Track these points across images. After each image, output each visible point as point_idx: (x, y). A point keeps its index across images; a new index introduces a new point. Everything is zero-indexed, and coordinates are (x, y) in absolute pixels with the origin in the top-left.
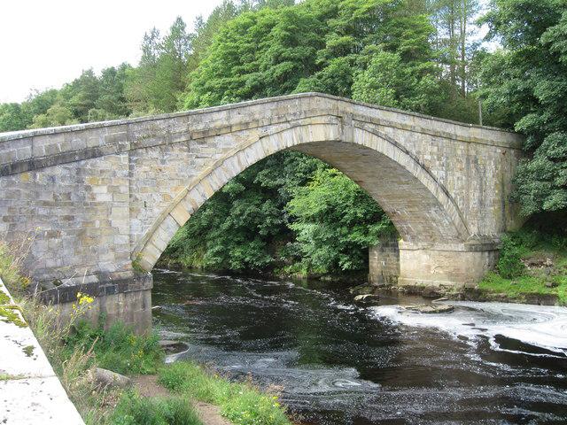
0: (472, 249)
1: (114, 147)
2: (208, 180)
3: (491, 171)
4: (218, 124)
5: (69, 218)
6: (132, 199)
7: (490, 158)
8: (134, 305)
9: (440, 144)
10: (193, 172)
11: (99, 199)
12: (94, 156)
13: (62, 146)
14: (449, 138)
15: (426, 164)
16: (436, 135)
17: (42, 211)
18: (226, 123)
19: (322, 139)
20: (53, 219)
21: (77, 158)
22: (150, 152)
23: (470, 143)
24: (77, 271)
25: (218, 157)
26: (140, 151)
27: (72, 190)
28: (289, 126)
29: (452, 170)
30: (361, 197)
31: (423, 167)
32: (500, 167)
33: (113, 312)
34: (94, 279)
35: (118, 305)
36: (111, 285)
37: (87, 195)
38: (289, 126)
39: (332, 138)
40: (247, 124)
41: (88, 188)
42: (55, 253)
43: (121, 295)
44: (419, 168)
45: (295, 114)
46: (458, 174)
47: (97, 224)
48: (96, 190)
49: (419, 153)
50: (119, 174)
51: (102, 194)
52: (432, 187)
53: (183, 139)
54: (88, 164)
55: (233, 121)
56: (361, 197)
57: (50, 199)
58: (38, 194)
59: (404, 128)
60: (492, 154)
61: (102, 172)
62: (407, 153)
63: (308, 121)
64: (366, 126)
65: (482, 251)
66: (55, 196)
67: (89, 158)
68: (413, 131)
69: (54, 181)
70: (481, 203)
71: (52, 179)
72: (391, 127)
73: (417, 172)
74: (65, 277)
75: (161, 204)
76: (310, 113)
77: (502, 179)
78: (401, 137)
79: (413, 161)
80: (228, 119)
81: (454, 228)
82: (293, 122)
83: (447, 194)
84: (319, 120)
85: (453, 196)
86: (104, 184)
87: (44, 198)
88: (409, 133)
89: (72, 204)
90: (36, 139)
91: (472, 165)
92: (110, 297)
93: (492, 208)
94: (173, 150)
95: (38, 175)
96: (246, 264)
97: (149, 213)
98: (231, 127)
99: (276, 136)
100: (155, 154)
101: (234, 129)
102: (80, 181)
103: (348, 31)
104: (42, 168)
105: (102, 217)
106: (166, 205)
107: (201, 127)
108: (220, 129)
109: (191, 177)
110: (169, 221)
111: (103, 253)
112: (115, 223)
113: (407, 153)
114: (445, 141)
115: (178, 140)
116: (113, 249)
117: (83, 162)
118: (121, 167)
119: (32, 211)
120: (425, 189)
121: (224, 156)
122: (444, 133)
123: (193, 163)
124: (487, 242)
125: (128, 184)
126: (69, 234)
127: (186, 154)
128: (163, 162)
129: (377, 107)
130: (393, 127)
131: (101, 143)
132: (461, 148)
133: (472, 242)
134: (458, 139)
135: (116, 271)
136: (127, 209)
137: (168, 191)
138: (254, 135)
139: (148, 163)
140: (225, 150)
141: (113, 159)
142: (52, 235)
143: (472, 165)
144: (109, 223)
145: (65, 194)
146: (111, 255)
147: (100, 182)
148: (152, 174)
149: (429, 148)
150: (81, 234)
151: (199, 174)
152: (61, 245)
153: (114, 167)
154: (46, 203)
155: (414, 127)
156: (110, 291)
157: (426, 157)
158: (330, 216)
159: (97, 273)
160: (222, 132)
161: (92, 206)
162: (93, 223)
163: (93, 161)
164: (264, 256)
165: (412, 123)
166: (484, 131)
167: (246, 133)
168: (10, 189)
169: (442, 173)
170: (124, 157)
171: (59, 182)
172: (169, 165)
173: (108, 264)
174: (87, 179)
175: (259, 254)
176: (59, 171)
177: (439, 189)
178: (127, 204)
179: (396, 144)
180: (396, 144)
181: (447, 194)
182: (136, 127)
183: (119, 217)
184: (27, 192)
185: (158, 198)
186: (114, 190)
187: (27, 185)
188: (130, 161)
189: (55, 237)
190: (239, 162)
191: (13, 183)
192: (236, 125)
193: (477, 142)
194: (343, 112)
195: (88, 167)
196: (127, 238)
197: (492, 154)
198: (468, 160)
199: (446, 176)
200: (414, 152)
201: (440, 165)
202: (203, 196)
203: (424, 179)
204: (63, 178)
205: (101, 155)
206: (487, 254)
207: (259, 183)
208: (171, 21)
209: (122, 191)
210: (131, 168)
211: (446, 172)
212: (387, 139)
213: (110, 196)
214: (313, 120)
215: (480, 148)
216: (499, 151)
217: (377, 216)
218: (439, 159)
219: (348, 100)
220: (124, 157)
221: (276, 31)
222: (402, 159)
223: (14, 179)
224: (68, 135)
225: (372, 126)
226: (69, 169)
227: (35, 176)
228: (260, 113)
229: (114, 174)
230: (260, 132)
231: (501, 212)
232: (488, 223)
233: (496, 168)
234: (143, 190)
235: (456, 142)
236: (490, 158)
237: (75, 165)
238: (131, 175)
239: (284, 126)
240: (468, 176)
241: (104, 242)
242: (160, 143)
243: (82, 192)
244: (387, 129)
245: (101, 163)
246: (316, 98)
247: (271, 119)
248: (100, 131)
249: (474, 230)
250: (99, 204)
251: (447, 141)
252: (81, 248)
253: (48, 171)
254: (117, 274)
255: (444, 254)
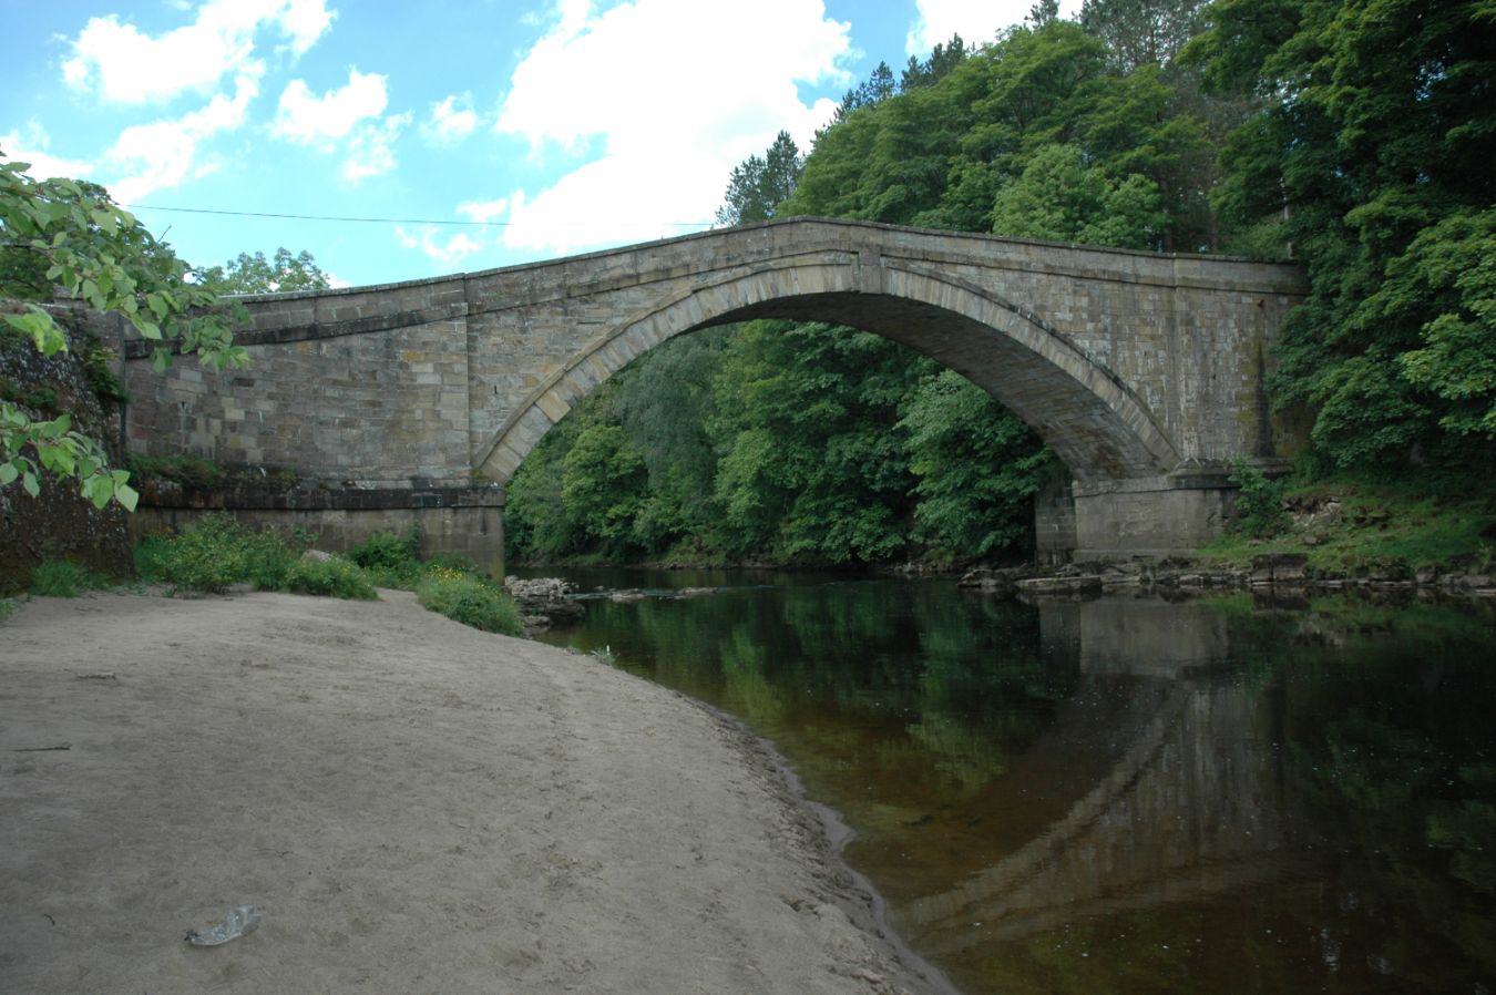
0: (1183, 483)
1: (444, 311)
2: (600, 357)
3: (1229, 341)
4: (617, 273)
5: (373, 404)
6: (475, 383)
7: (1225, 314)
8: (469, 526)
9: (1096, 293)
10: (575, 345)
11: (421, 380)
12: (412, 323)
13: (363, 310)
14: (1121, 280)
15: (1062, 329)
16: (1082, 276)
17: (330, 392)
18: (631, 271)
19: (820, 289)
20: (349, 403)
21: (385, 325)
22: (503, 317)
23: (1174, 288)
24: (382, 473)
25: (617, 321)
26: (487, 315)
27: (378, 367)
28: (749, 271)
29: (1131, 338)
30: (998, 410)
31: (1053, 333)
32: (1251, 330)
33: (438, 533)
34: (407, 485)
35: (443, 523)
36: (431, 494)
37: (402, 374)
38: (749, 271)
39: (839, 286)
40: (668, 270)
41: (403, 366)
42: (352, 449)
43: (448, 511)
44: (1044, 337)
45: (760, 253)
46: (1148, 346)
47: (418, 414)
48: (415, 368)
49: (1042, 308)
50: (452, 348)
51: (426, 374)
52: (1077, 370)
53: (555, 296)
54: (404, 334)
55: (641, 269)
56: (998, 410)
57: (345, 377)
58: (324, 370)
59: (1002, 266)
60: (1232, 306)
61: (425, 344)
62: (1012, 309)
63: (788, 262)
64: (912, 266)
65: (1205, 489)
66: (350, 374)
67: (404, 326)
68: (1024, 269)
69: (349, 354)
70: (1205, 398)
71: (348, 352)
72: (972, 265)
73: (1040, 343)
74: (363, 479)
75: (521, 391)
76: (794, 250)
77: (1260, 353)
78: (997, 283)
79: (1027, 323)
80: (634, 264)
81: (1141, 447)
82: (757, 265)
83: (1116, 381)
84: (809, 260)
85: (1134, 386)
86: (426, 361)
87: (333, 375)
88: (1017, 274)
89: (379, 386)
90: (320, 301)
91: (1180, 329)
92: (430, 512)
93: (1235, 410)
94: (539, 313)
95: (325, 346)
96: (855, 550)
97: (503, 403)
98: (638, 276)
99: (725, 289)
100: (511, 319)
101: (643, 280)
102: (391, 356)
103: (1001, 114)
104: (330, 337)
105: (428, 405)
106: (529, 391)
107: (586, 279)
108: (618, 280)
109: (570, 351)
110: (535, 413)
111: (428, 454)
112: (446, 414)
113: (1012, 309)
114: (1107, 286)
115: (547, 299)
116: (444, 450)
117: (395, 332)
118: (455, 338)
119: (315, 392)
120: (1063, 373)
121: (627, 320)
122: (1104, 272)
123: (573, 331)
124: (1215, 471)
125: (465, 361)
126: (373, 424)
127: (560, 318)
128: (524, 330)
129: (956, 233)
130: (979, 266)
131: (424, 305)
132: (1149, 301)
133: (1179, 472)
134: (1141, 281)
135: (443, 479)
136: (464, 396)
137: (532, 371)
138: (683, 288)
139: (500, 332)
140: (628, 312)
141: (442, 327)
142: (345, 424)
143: (1180, 329)
144: (437, 415)
145: (366, 372)
146: (442, 457)
147: (422, 358)
148: (506, 348)
149: (1068, 301)
150: (394, 425)
151: (585, 348)
152: (361, 438)
153: (444, 338)
154: (336, 383)
155: (1028, 264)
156: (430, 504)
157: (1059, 315)
158: (956, 444)
159: (414, 479)
160: (622, 285)
161: (411, 390)
162: (412, 412)
163: (409, 329)
164: (886, 534)
165: (1023, 257)
166: (1208, 265)
167: (666, 285)
168: (280, 360)
169: (1105, 344)
170: (459, 326)
171: (357, 356)
172: (532, 334)
173: (436, 470)
174: (402, 354)
175: (880, 530)
176: (357, 341)
177: (1096, 374)
178: (465, 388)
179: (983, 294)
180: (983, 294)
181: (1116, 381)
182: (481, 284)
183: (453, 405)
184: (308, 366)
185: (516, 382)
186: (443, 369)
187: (306, 358)
188: (469, 329)
189: (352, 427)
190: (656, 329)
191: (284, 353)
192: (648, 273)
193: (1189, 286)
194: (860, 245)
195: (405, 337)
196: (465, 435)
197: (1232, 306)
198: (1171, 322)
199: (1114, 349)
200: (1029, 306)
201: (1096, 330)
202: (592, 379)
203: (1057, 356)
204: (365, 351)
205: (422, 322)
206: (1216, 494)
207: (867, 401)
208: (749, 157)
209: (456, 371)
210: (471, 339)
211: (1114, 342)
212: (961, 284)
213: (438, 377)
214: (798, 261)
215: (1196, 296)
216: (1247, 300)
217: (1032, 440)
218: (1093, 318)
219: (904, 228)
220: (459, 326)
221: (883, 135)
222: (1000, 320)
223: (285, 348)
224: (372, 297)
225: (926, 265)
226: (373, 339)
227: (320, 348)
228: (692, 254)
229: (444, 348)
230: (693, 282)
231: (1255, 419)
232: (1226, 438)
233: (1242, 333)
234: (493, 371)
235: (1137, 289)
236: (1225, 314)
237: (383, 334)
238: (470, 348)
239: (740, 272)
240: (1173, 351)
241: (428, 440)
242: (518, 303)
243: (393, 370)
244: (962, 270)
245: (424, 333)
246: (804, 225)
247: (714, 261)
248: (423, 290)
249: (1189, 450)
250: (422, 386)
251: (1116, 286)
252: (393, 445)
253: (341, 342)
254: (442, 483)
255: (1140, 497)
